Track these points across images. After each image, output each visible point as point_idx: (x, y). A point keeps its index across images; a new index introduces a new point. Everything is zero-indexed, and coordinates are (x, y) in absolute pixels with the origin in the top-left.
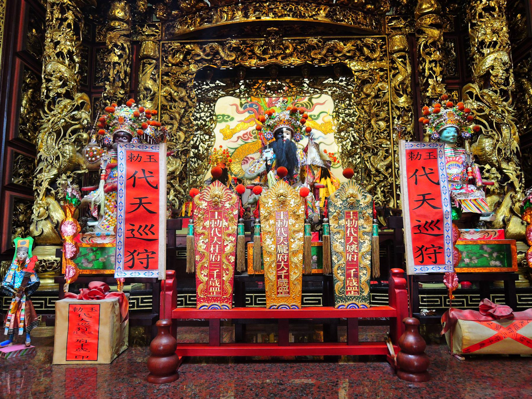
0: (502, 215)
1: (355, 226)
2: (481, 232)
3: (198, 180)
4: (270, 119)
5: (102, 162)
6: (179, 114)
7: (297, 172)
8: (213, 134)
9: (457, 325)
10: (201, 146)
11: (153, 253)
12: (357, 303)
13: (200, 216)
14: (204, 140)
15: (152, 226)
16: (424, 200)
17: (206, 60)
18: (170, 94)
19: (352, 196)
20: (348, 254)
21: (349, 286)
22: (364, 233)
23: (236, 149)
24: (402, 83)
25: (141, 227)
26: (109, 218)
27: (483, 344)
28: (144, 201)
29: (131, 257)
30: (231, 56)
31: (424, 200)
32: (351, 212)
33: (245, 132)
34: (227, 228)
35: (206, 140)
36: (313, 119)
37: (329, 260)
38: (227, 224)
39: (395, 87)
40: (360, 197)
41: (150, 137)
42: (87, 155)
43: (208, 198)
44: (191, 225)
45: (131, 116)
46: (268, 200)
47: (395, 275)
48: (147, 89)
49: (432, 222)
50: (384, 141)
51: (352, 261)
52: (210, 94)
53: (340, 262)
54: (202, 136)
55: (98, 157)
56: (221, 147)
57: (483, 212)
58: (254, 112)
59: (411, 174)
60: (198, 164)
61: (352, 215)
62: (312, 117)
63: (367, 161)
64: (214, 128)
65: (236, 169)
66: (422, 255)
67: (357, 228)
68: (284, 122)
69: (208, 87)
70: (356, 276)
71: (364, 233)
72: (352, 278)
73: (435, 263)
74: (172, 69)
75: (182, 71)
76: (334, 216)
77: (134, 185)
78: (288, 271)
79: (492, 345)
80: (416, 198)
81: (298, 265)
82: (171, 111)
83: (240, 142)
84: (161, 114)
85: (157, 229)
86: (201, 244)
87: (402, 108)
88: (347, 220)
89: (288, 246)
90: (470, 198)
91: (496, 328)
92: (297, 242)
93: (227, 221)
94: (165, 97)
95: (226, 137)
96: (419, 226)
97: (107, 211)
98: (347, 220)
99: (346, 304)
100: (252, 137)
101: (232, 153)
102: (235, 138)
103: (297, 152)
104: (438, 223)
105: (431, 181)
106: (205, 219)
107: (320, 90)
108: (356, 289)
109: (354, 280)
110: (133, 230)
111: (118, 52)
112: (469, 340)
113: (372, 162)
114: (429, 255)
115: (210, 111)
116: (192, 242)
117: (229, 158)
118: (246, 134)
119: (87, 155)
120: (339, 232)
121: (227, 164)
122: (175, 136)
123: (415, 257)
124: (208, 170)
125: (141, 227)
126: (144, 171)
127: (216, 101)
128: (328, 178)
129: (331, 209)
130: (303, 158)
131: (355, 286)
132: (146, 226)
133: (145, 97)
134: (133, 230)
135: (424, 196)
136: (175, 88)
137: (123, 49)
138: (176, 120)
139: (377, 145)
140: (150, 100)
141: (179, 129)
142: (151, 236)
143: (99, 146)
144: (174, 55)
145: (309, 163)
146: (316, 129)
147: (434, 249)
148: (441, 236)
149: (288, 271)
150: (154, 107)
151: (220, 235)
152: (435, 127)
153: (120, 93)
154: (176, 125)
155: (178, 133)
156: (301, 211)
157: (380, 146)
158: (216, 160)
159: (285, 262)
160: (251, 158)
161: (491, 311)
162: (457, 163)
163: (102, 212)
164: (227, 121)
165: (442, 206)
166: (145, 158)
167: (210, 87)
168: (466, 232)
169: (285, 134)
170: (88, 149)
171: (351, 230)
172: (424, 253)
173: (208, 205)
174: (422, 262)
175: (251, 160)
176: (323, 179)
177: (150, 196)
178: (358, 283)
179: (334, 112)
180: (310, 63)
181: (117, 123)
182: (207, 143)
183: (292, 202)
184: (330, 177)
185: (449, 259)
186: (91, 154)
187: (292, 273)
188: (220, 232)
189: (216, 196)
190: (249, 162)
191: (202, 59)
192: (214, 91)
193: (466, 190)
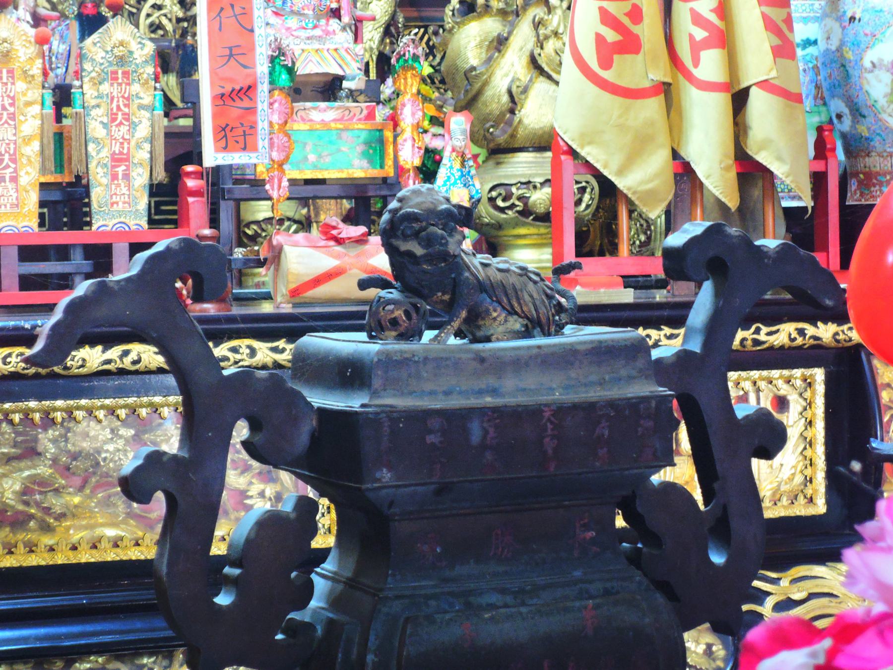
0: (506, 75)
1: (126, 95)
2: (338, 108)
9: (283, 255)
12: (127, 221)
19: (121, 44)
20: (114, 142)
21: (115, 194)
22: (141, 107)
27: (317, 281)
31: (231, 55)
32: (120, 72)
37: (83, 151)
40: (134, 46)
47: (189, 174)
49: (241, 89)
51: (121, 153)
53: (101, 155)
57: (348, 72)
59: (214, 15)
61: (120, 75)
66: (227, 136)
67: (128, 99)
70: (127, 176)
71: (141, 107)
72: (120, 182)
73: (244, 149)
76: (92, 78)
78: (15, 170)
80: (220, 52)
81: (32, 160)
88: (112, 85)
89: (15, 128)
90: (327, 46)
91: (338, 256)
96: (223, 95)
98: (112, 85)
99: (111, 224)
104: (249, 90)
105: (244, 28)
108: (127, 199)
109: (123, 185)
114: (237, 139)
120: (98, 106)
123: (217, 140)
129: (87, 66)
131: (124, 194)
135: (231, 49)
147: (244, 129)
148: (252, 111)
149: (15, 170)
156: (36, 69)
159: (10, 155)
161: (334, 232)
171: (118, 101)
172: (229, 134)
174: (225, 149)
178: (129, 189)
185: (262, 143)
187: (22, 173)
193: (323, 31)
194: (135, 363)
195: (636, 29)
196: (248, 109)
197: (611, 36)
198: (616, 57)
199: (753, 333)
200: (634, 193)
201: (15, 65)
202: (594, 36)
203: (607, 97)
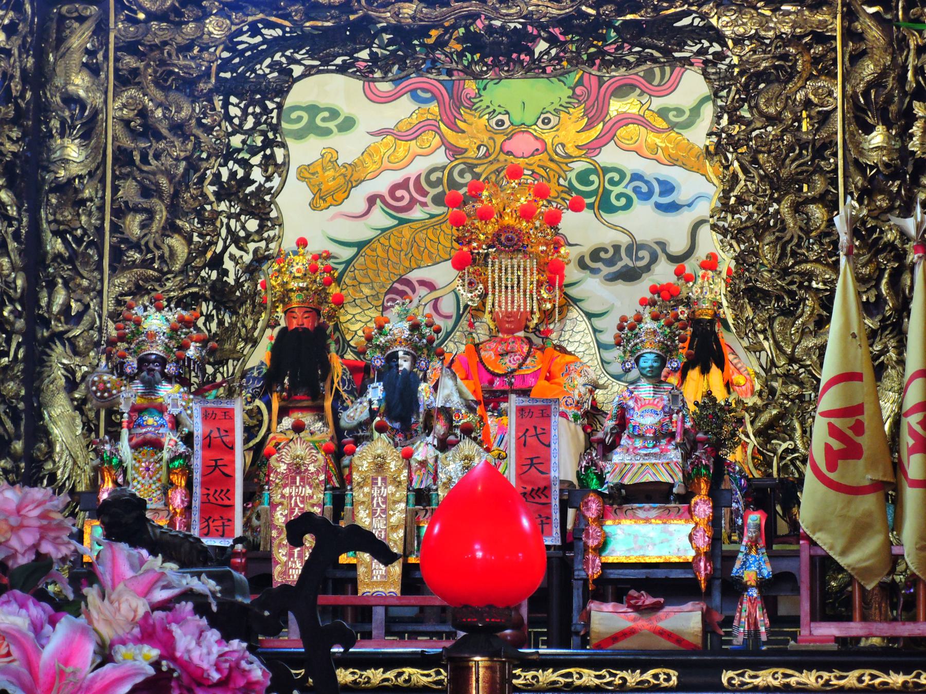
2: (659, 508)
3: (219, 379)
4: (380, 334)
5: (122, 400)
6: (171, 178)
8: (273, 214)
10: (232, 257)
11: (229, 520)
13: (277, 481)
14: (242, 234)
15: (228, 490)
16: (532, 465)
18: (143, 113)
23: (361, 245)
24: (877, 83)
25: (216, 491)
26: (139, 486)
28: (219, 463)
29: (206, 524)
33: (398, 177)
34: (311, 497)
35: (249, 235)
36: (672, 126)
38: (310, 492)
39: (854, 96)
41: (195, 363)
42: (94, 388)
43: (288, 460)
44: (266, 493)
45: (165, 328)
48: (70, 100)
49: (539, 489)
50: (819, 269)
52: (263, 68)
54: (233, 222)
55: (114, 392)
56: (302, 242)
58: (434, 97)
59: (521, 434)
60: (221, 323)
62: (671, 116)
63: (763, 331)
64: (278, 192)
68: (400, 342)
69: (259, 39)
74: (148, 30)
75: (179, 39)
77: (209, 446)
79: (628, 639)
82: (146, 168)
83: (380, 218)
84: (115, 177)
85: (234, 494)
86: (279, 516)
87: (872, 168)
91: (634, 620)
92: (397, 515)
93: (311, 488)
94: (126, 123)
95: (322, 198)
97: (136, 476)
100: (428, 199)
101: (348, 263)
102: (357, 201)
103: (420, 389)
106: (285, 486)
107: (666, 52)
110: (208, 495)
112: (599, 633)
113: (779, 337)
115: (264, 127)
116: (267, 514)
117: (334, 289)
118: (404, 185)
119: (94, 388)
121: (325, 309)
122: (159, 248)
124: (255, 343)
125: (216, 491)
126: (219, 429)
127: (288, 92)
128: (714, 369)
130: (429, 398)
132: (222, 491)
134: (208, 495)
135: (531, 459)
136: (159, 95)
138: (161, 198)
139: (792, 283)
140: (81, 137)
141: (171, 228)
142: (227, 502)
143: (113, 374)
145: (439, 404)
146: (683, 166)
150: (94, 159)
151: (302, 506)
152: (630, 352)
153: (10, 138)
154: (162, 215)
155: (168, 241)
156: (404, 475)
158: (285, 297)
160: (423, 283)
162: (655, 408)
163: (129, 477)
164: (327, 132)
165: (550, 471)
166: (220, 415)
167: (265, 41)
168: (640, 508)
169: (400, 362)
170: (96, 379)
173: (288, 468)
175: (422, 291)
176: (694, 374)
177: (226, 458)
179: (710, 134)
180: (592, 11)
181: (143, 341)
182: (252, 246)
183: (392, 465)
184: (721, 365)
186: (101, 386)
188: (302, 502)
189: (298, 457)
192: (277, 57)
194: (406, 681)
195: (859, 440)
196: (544, 504)
197: (836, 445)
198: (840, 462)
199: (914, 677)
200: (853, 569)
201: (388, 474)
202: (823, 446)
203: (832, 493)
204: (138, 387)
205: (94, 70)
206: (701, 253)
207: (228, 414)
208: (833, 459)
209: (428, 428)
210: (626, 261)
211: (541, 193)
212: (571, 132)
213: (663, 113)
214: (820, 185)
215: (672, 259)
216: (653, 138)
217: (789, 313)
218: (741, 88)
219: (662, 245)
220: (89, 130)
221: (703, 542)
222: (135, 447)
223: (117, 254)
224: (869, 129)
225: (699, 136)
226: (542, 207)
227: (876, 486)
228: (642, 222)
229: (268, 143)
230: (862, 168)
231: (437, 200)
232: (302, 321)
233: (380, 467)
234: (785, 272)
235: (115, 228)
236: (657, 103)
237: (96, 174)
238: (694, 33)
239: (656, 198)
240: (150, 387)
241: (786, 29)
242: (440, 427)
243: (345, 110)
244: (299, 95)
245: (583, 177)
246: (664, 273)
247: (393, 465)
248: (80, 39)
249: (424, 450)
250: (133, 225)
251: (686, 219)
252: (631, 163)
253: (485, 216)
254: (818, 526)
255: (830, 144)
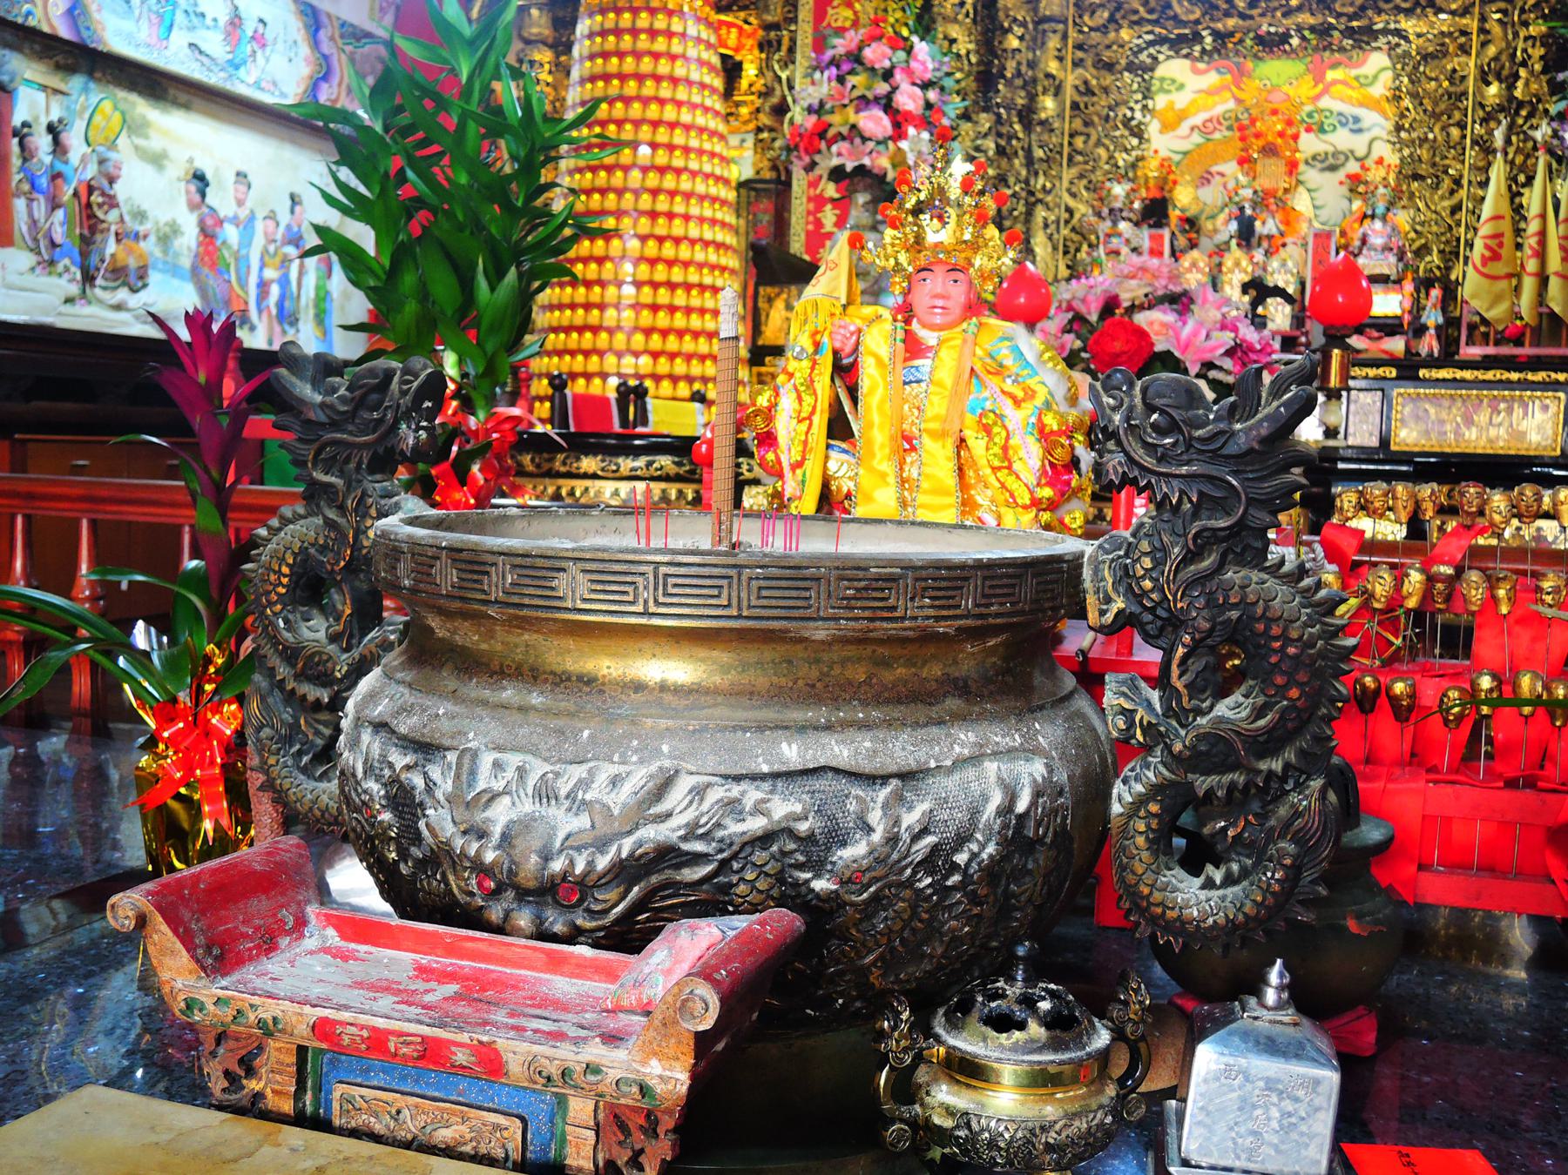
7: (1254, 241)
17: (1149, 21)
18: (1086, 83)
23: (1185, 153)
24: (1496, 59)
30: (1193, 12)
36: (1362, 85)
46: (1228, 262)
50: (1453, 163)
52: (1143, 57)
65: (1184, 197)
83: (1197, 138)
94: (1076, 87)
95: (1167, 127)
111: (1018, 31)
117: (1172, 177)
118: (1210, 120)
133: (1045, 92)
136: (1094, 72)
137: (1024, 24)
144: (1093, 13)
157: (1446, 172)
164: (1168, 92)
175: (1218, 179)
190: (1213, 181)
191: (1142, 19)
197: (1487, 254)
204: (1108, 223)
205: (1060, 59)
206: (1375, 155)
207: (1161, 237)
208: (1485, 261)
209: (1259, 245)
210: (1331, 161)
211: (1290, 123)
212: (1306, 89)
213: (1357, 78)
214: (1457, 115)
215: (1357, 159)
216: (1350, 92)
217: (1437, 187)
218: (1414, 65)
219: (1352, 152)
220: (1058, 91)
221: (1407, 306)
222: (1108, 254)
223: (1070, 159)
224: (1488, 84)
225: (1380, 89)
226: (1290, 132)
227: (1509, 276)
228: (1342, 139)
229: (1145, 98)
230: (1482, 106)
231: (1230, 128)
232: (1155, 194)
233: (1237, 264)
234: (1434, 165)
235: (1070, 144)
236: (1354, 72)
237: (1061, 116)
238: (1385, 32)
239: (1351, 126)
240: (1115, 223)
241: (1445, 29)
242: (1265, 244)
243: (1180, 79)
244: (1160, 71)
245: (1310, 115)
246: (1353, 167)
247: (1244, 263)
248: (1053, 42)
249: (1259, 255)
250: (1079, 142)
251: (1366, 137)
252: (1337, 106)
253: (1258, 136)
254: (1474, 296)
255: (1465, 94)
